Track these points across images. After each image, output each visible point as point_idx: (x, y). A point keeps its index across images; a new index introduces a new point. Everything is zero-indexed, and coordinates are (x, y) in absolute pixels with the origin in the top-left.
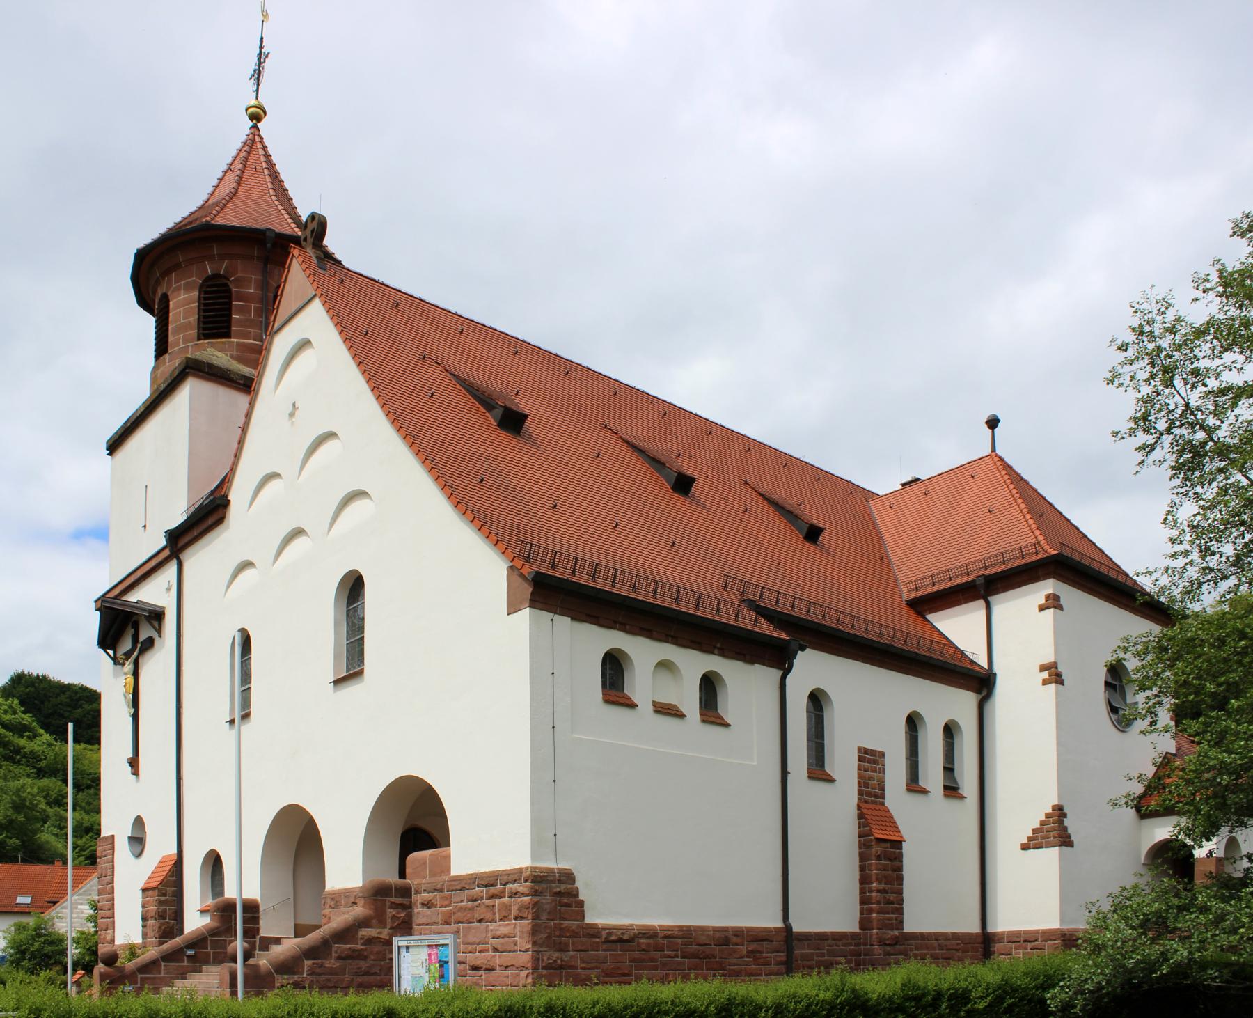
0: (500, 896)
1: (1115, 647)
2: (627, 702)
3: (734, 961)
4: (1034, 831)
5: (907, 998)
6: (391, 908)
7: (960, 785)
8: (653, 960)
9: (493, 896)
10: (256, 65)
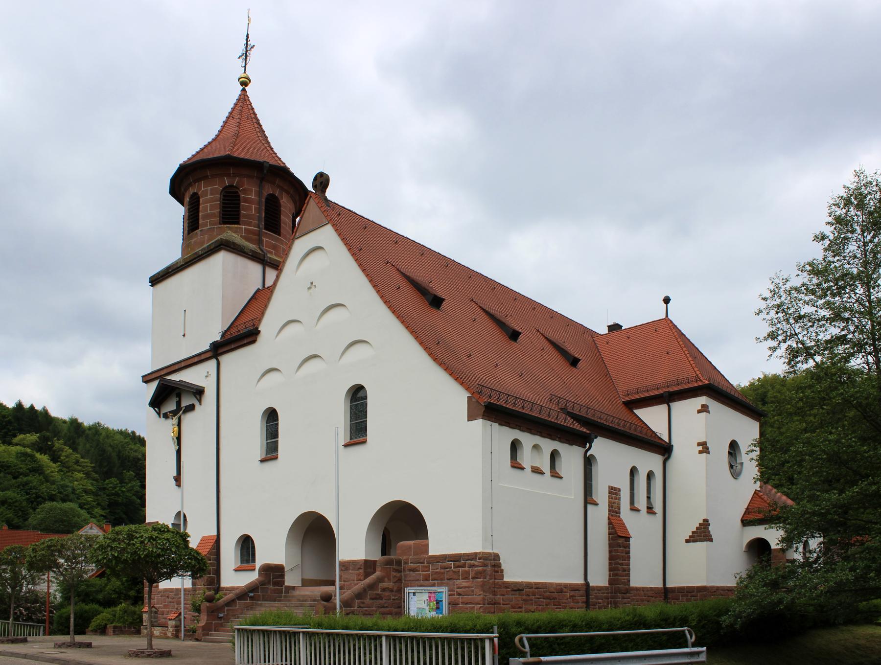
0: (464, 566)
1: (750, 444)
2: (519, 466)
3: (564, 601)
4: (693, 532)
5: (662, 620)
6: (393, 572)
7: (654, 506)
8: (531, 600)
9: (459, 567)
10: (243, 50)
